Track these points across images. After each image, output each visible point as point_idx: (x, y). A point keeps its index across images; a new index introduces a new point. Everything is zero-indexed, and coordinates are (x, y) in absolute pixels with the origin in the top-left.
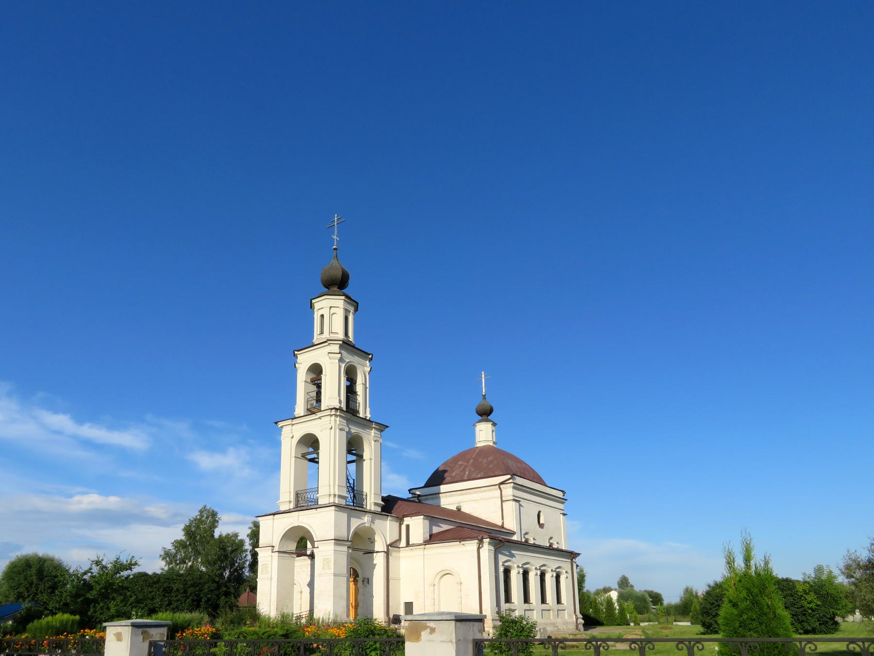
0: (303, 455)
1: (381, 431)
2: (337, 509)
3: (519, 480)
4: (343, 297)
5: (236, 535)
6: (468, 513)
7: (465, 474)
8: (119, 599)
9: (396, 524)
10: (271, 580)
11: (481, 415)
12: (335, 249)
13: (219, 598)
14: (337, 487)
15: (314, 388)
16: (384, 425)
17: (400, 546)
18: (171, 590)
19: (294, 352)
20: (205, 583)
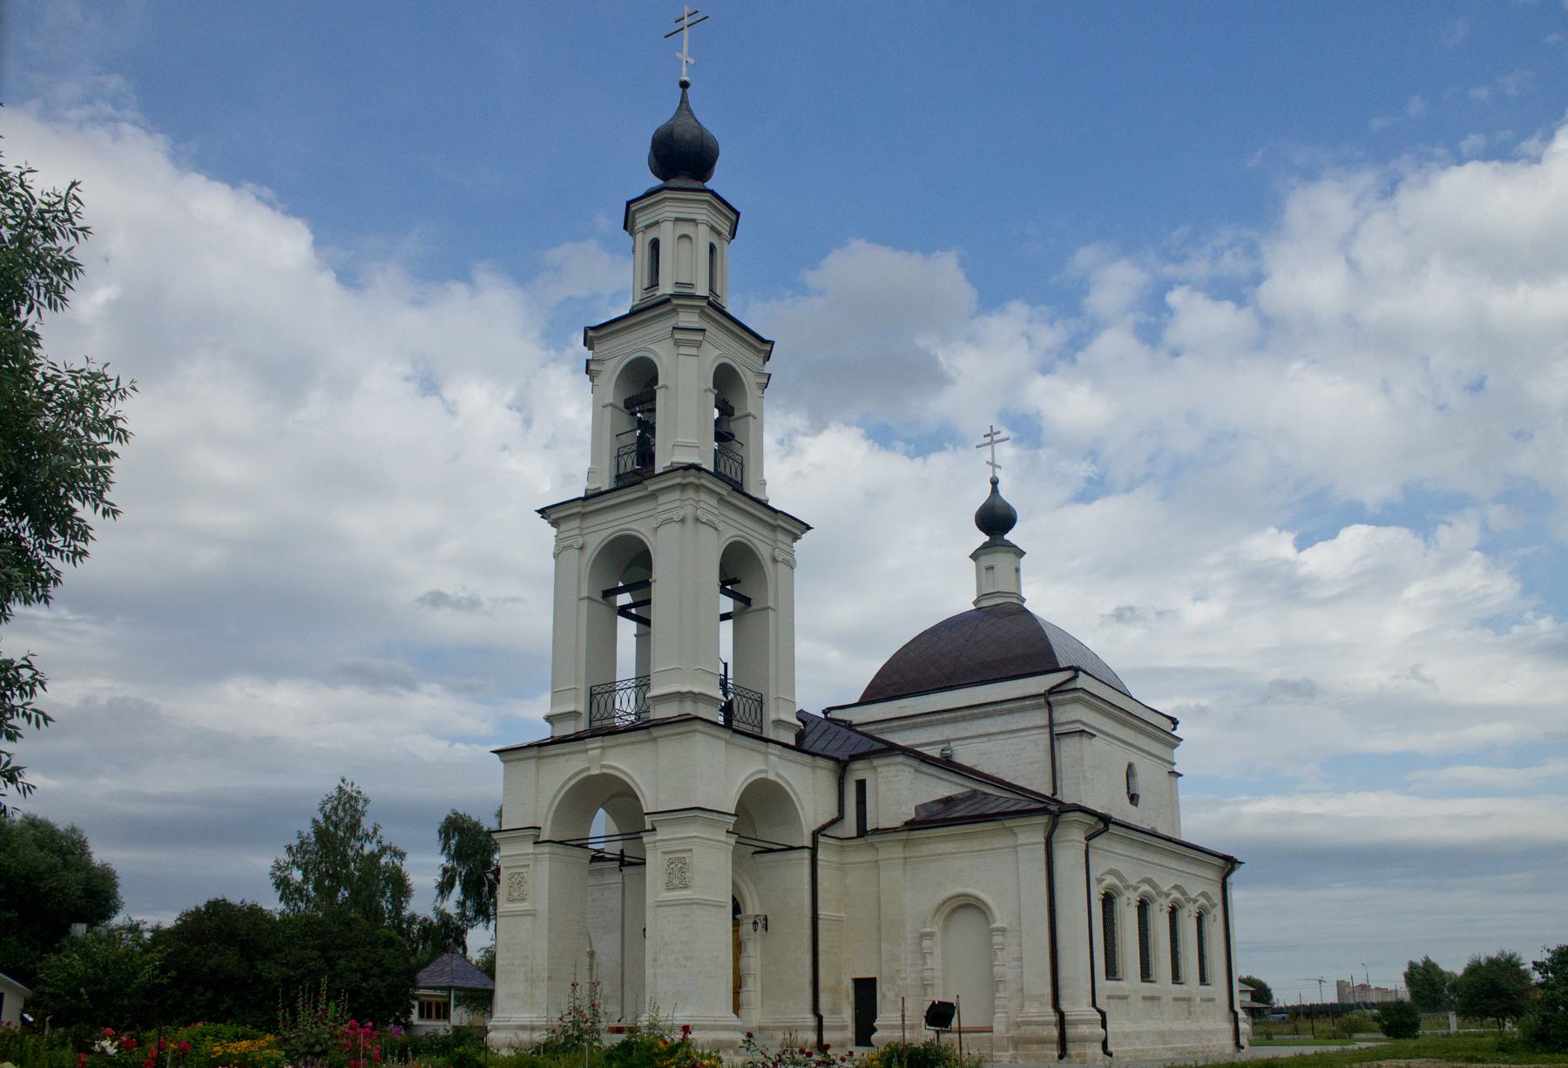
6: (968, 765)
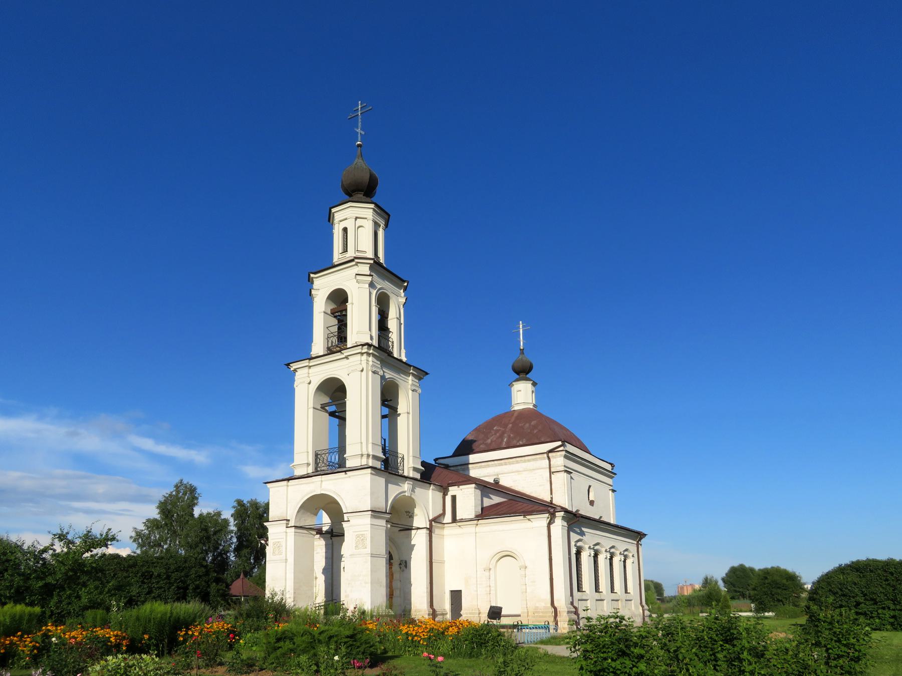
0: (323, 406)
1: (420, 379)
2: (373, 472)
3: (570, 448)
4: (372, 206)
5: (219, 514)
7: (502, 440)
8: (91, 585)
9: (440, 495)
10: (286, 562)
11: (518, 373)
12: (359, 146)
13: (209, 586)
14: (370, 446)
15: (335, 321)
16: (423, 371)
17: (444, 522)
18: (151, 576)
19: (309, 275)
20: (191, 568)
